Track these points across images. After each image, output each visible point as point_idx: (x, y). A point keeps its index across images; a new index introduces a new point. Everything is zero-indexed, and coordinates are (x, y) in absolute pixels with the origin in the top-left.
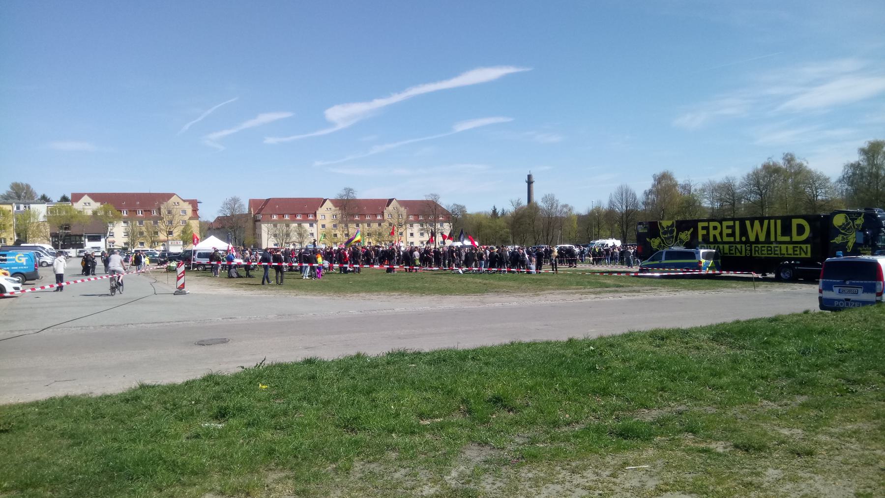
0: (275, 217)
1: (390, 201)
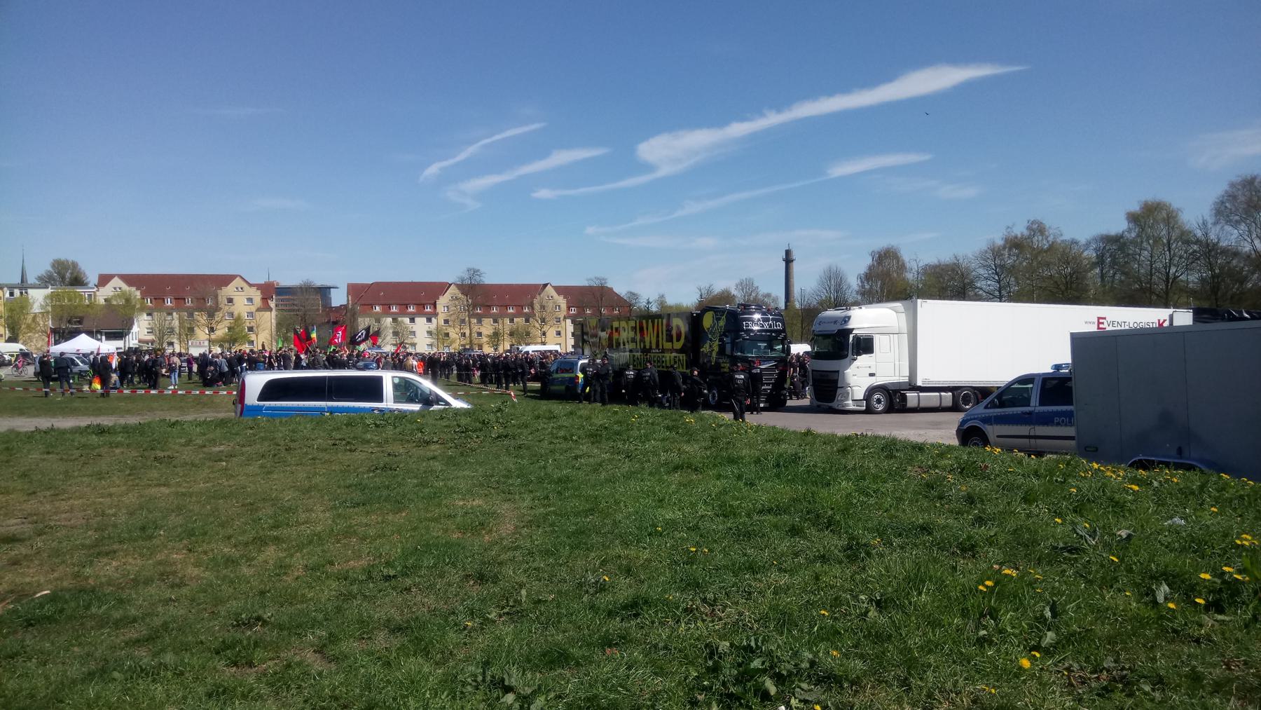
0: (378, 309)
1: (545, 285)
